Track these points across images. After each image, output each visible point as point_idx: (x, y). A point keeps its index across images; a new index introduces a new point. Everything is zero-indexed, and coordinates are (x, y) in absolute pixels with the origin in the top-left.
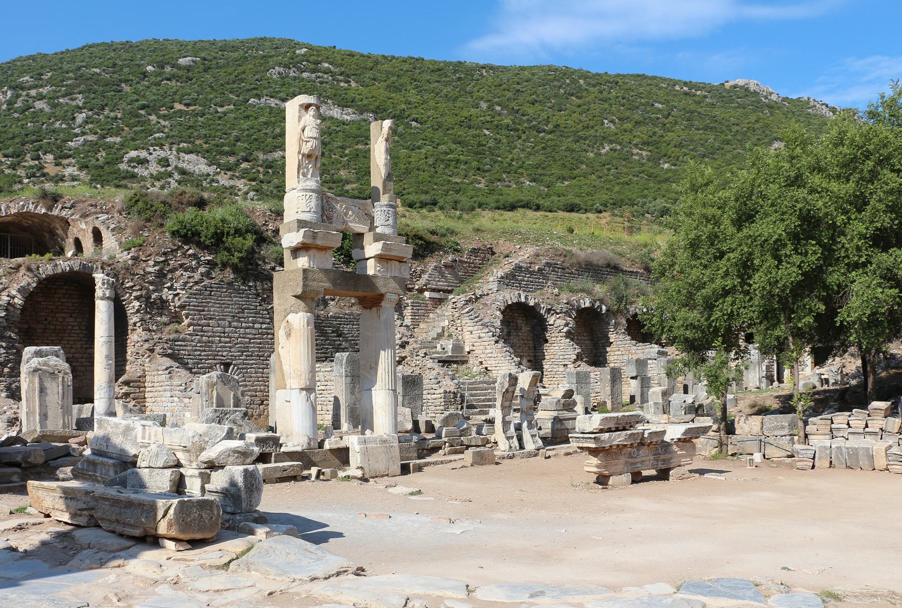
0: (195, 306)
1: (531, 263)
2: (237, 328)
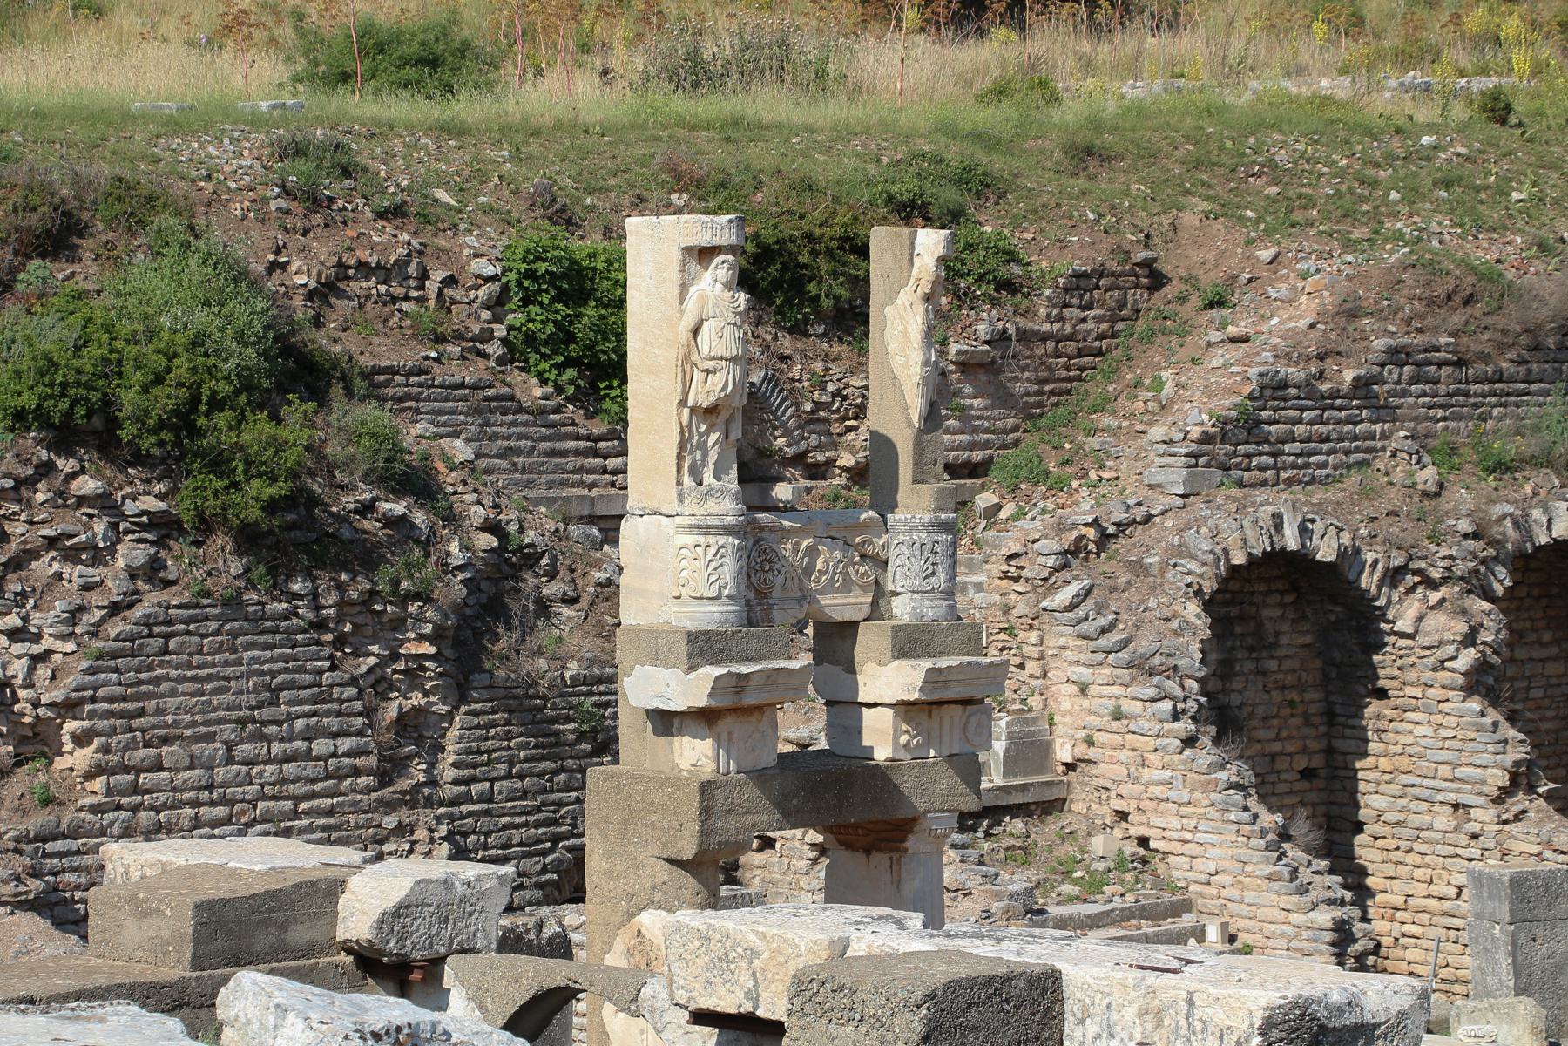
0: (111, 700)
1: (1321, 358)
2: (251, 763)
